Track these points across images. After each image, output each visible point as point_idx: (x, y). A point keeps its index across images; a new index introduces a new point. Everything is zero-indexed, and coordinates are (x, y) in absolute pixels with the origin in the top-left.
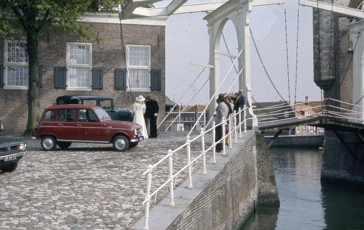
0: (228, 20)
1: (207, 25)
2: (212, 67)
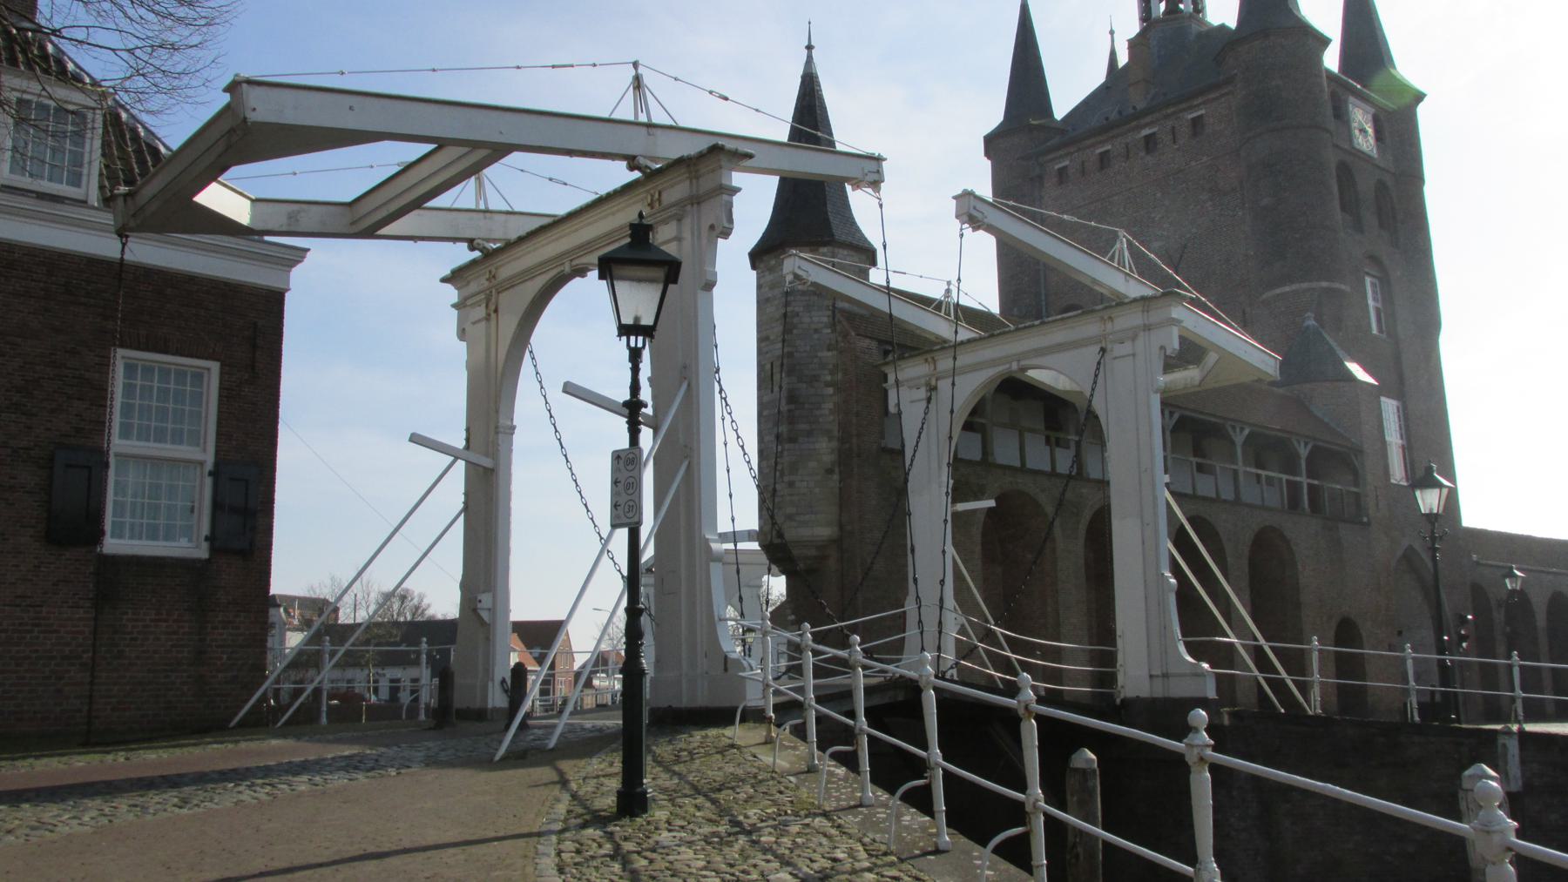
2: (486, 462)
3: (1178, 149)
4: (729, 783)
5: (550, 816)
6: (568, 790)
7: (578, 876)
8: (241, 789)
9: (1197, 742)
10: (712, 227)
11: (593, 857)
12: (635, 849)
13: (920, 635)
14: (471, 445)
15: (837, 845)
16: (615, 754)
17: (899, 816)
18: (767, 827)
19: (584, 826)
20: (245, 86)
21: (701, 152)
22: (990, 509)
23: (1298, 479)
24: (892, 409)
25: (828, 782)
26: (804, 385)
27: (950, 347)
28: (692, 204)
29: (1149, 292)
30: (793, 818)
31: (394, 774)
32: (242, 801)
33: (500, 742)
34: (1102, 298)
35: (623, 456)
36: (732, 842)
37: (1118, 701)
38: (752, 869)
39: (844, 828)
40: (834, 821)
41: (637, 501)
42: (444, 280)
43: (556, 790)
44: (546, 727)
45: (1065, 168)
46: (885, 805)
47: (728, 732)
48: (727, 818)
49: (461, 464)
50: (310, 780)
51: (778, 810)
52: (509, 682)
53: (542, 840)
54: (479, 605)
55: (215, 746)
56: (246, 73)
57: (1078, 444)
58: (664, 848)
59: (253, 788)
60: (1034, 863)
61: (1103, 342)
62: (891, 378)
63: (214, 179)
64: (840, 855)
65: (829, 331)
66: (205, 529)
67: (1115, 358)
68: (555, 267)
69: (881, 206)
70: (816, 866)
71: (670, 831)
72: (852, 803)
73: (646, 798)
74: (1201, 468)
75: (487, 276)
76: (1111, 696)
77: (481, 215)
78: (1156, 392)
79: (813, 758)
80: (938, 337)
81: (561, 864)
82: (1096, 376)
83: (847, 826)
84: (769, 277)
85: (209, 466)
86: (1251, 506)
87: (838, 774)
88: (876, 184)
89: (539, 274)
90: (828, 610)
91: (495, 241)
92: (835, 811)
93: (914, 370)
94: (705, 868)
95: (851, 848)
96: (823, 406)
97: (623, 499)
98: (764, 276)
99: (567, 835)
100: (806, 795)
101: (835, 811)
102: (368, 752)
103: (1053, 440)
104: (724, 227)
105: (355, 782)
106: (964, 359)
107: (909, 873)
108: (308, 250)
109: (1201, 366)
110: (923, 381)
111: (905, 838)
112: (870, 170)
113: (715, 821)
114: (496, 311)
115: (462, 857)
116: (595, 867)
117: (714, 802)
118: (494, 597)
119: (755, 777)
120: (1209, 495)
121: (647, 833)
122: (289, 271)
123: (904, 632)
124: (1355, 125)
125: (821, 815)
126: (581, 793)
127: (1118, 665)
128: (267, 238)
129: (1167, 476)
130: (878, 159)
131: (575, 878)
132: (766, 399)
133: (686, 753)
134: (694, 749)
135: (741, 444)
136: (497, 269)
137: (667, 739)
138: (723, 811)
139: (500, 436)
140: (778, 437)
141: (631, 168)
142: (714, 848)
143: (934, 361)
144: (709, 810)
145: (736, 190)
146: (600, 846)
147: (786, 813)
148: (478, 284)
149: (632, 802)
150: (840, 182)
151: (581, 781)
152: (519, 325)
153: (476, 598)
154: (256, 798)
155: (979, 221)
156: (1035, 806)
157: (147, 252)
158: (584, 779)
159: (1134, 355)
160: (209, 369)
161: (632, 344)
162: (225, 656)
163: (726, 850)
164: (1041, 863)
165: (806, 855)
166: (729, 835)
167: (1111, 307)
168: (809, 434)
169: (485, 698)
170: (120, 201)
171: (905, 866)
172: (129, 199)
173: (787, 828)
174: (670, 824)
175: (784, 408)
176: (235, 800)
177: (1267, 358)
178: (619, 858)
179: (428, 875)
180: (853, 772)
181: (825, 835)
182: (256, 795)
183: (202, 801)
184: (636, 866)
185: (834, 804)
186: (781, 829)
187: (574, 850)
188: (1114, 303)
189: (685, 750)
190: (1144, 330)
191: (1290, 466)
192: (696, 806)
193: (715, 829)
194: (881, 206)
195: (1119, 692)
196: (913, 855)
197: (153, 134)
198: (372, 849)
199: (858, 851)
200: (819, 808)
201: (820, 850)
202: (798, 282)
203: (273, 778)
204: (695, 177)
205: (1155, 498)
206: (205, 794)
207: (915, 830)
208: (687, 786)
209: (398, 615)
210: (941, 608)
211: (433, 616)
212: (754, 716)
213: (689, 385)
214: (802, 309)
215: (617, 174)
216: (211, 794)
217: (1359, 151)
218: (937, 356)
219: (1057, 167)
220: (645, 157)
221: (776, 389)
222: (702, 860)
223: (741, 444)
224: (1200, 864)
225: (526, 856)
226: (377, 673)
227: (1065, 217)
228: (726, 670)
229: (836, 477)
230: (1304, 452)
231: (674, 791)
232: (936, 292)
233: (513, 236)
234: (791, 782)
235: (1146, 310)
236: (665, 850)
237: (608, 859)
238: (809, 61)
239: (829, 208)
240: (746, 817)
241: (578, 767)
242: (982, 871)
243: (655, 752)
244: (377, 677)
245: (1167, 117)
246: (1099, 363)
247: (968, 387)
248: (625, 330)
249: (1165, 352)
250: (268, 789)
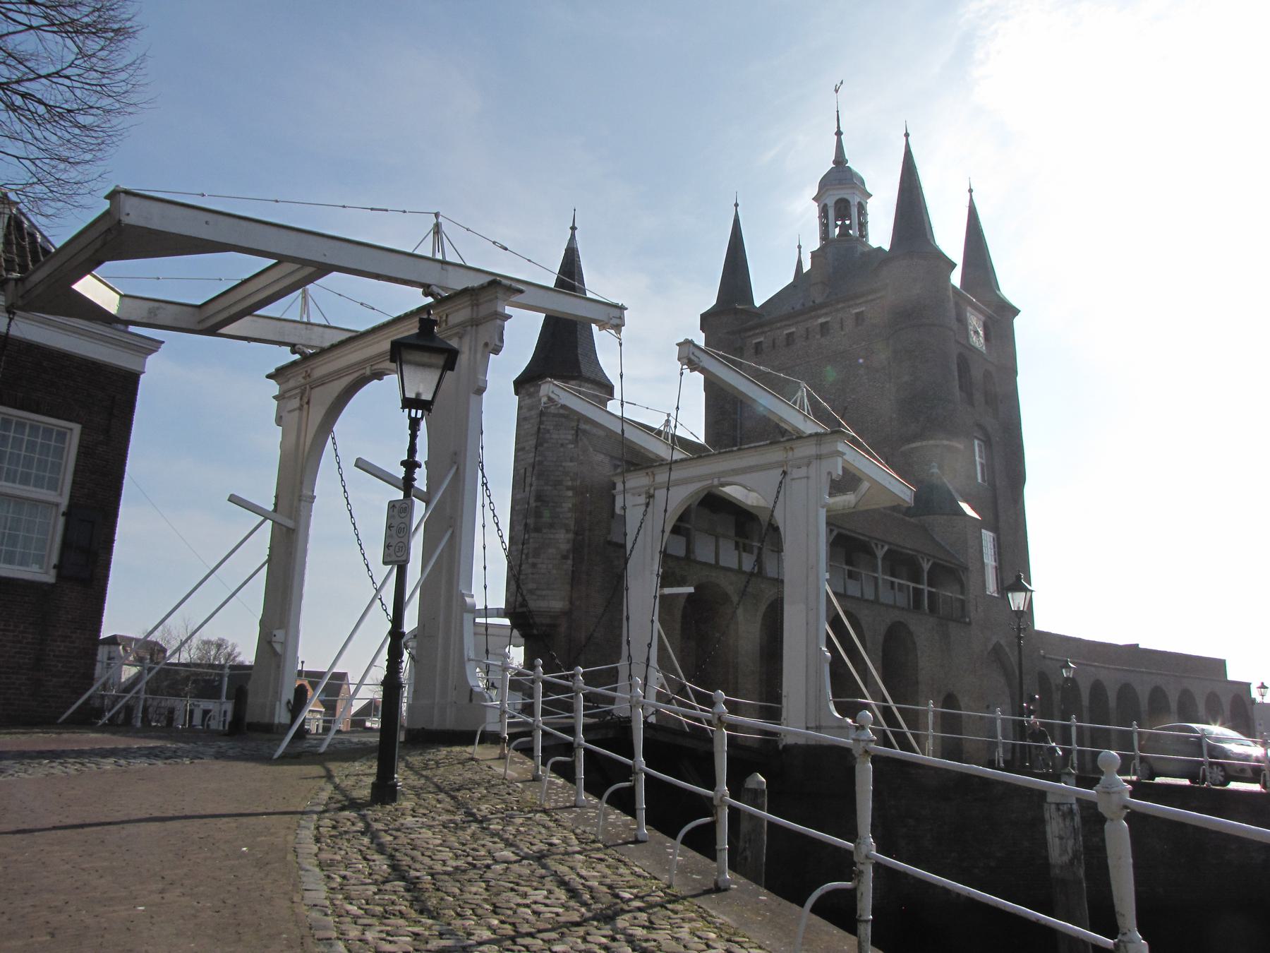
2: (290, 524)
3: (844, 335)
4: (467, 785)
5: (313, 801)
6: (332, 783)
7: (332, 845)
8: (54, 764)
9: (863, 737)
10: (486, 345)
11: (346, 832)
12: (383, 828)
13: (628, 666)
14: (278, 509)
15: (554, 834)
16: (374, 760)
17: (606, 815)
18: (496, 818)
19: (343, 809)
20: (122, 195)
21: (482, 285)
22: (690, 595)
23: (921, 587)
24: (618, 511)
25: (549, 788)
26: (550, 488)
27: (667, 464)
28: (472, 326)
29: (820, 430)
30: (518, 813)
31: (188, 762)
32: (53, 774)
33: (279, 746)
34: (783, 432)
35: (397, 505)
36: (465, 827)
37: (781, 747)
38: (480, 848)
39: (560, 821)
40: (552, 816)
41: (408, 524)
43: (322, 782)
44: (320, 739)
45: (760, 343)
46: (595, 807)
47: (469, 749)
48: (463, 810)
49: (269, 523)
50: (115, 762)
51: (506, 806)
52: (292, 702)
53: (304, 817)
54: (274, 639)
55: (41, 735)
56: (124, 186)
57: (760, 549)
58: (407, 829)
59: (65, 765)
60: (718, 847)
61: (785, 467)
62: (619, 487)
63: (89, 272)
64: (555, 841)
66: (54, 559)
67: (793, 479)
68: (358, 371)
69: (621, 345)
70: (534, 848)
71: (414, 817)
72: (568, 804)
73: (396, 790)
74: (851, 575)
75: (304, 375)
76: (776, 742)
77: (304, 326)
78: (823, 507)
79: (538, 769)
80: (657, 456)
81: (318, 835)
82: (778, 492)
83: (563, 820)
84: (528, 401)
85: (63, 508)
86: (887, 606)
87: (557, 783)
88: (618, 327)
89: (345, 375)
90: (557, 661)
91: (312, 347)
92: (553, 809)
93: (638, 481)
94: (441, 845)
95: (565, 837)
97: (396, 522)
98: (524, 400)
99: (327, 815)
100: (530, 797)
101: (553, 809)
102: (169, 745)
103: (741, 545)
104: (495, 345)
105: (154, 766)
106: (675, 475)
107: (613, 856)
108: (163, 342)
109: (855, 493)
110: (644, 490)
111: (610, 830)
112: (614, 317)
113: (453, 812)
114: (308, 403)
115: (235, 825)
116: (347, 839)
117: (453, 798)
118: (286, 634)
119: (489, 782)
120: (857, 595)
121: (394, 817)
122: (146, 358)
123: (617, 683)
124: (971, 327)
125: (541, 811)
126: (343, 785)
127: (782, 718)
128: (132, 329)
129: (828, 574)
130: (622, 308)
131: (329, 846)
132: (518, 497)
133: (433, 762)
134: (440, 760)
135: (496, 521)
136: (312, 369)
137: (419, 752)
138: (459, 805)
139: (303, 503)
140: (526, 525)
141: (426, 294)
142: (450, 831)
143: (654, 475)
144: (448, 803)
145: (509, 317)
146: (353, 824)
147: (512, 809)
148: (297, 380)
149: (384, 791)
150: (586, 324)
151: (344, 777)
152: (326, 412)
153: (271, 633)
154: (66, 773)
155: (696, 364)
156: (721, 800)
157: (30, 329)
158: (346, 776)
159: (808, 478)
160: (71, 429)
161: (413, 415)
162: (60, 665)
163: (460, 833)
164: (723, 847)
165: (527, 839)
166: (464, 822)
167: (793, 439)
168: (551, 526)
169: (273, 714)
170: (12, 284)
171: (609, 851)
172: (20, 284)
173: (512, 820)
174: (414, 811)
175: (533, 504)
176: (46, 773)
177: (906, 489)
178: (369, 834)
179: (202, 836)
180: (570, 782)
181: (544, 826)
182: (67, 770)
183: (17, 772)
184: (382, 840)
185: (553, 805)
186: (507, 820)
187: (331, 826)
188: (794, 437)
189: (432, 760)
190: (817, 459)
191: (916, 577)
192: (438, 800)
193: (452, 817)
194: (621, 345)
195: (782, 740)
196: (616, 843)
197: (49, 241)
198: (157, 814)
199: (571, 839)
200: (540, 806)
201: (539, 836)
202: (551, 404)
203: (84, 758)
204: (475, 305)
205: (818, 588)
206: (22, 767)
207: (619, 826)
208: (432, 785)
209: (214, 659)
210: (648, 666)
211: (242, 662)
212: (491, 738)
213: (458, 469)
214: (552, 428)
215: (415, 299)
216: (26, 767)
217: (973, 346)
218: (656, 470)
219: (754, 341)
220: (438, 286)
221: (527, 489)
222: (439, 839)
223: (496, 521)
224: (860, 839)
225: (289, 828)
226: (193, 704)
227: (761, 368)
228: (471, 700)
229: (570, 562)
230: (926, 566)
231: (421, 788)
232: (658, 424)
233: (327, 344)
234: (518, 787)
235: (819, 444)
236: (410, 830)
237: (359, 834)
238: (573, 236)
239: (580, 351)
240: (479, 810)
241: (343, 768)
242: (674, 857)
243: (407, 761)
244: (193, 707)
246: (781, 483)
247: (679, 497)
248: (408, 403)
249: (831, 477)
250: (78, 766)
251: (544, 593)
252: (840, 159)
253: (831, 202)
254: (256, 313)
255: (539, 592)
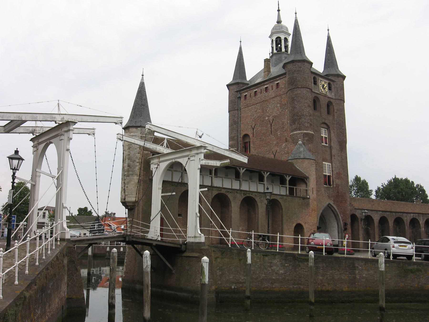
0: (51, 144)
1: (32, 146)
2: (34, 183)
26: (132, 162)
42: (30, 141)
65: (139, 149)
96: (136, 168)
114: (38, 149)
168: (132, 175)
194: (95, 138)
245: (271, 82)
251: (130, 195)
252: (279, 21)
253: (274, 39)
254: (20, 126)
255: (129, 196)
